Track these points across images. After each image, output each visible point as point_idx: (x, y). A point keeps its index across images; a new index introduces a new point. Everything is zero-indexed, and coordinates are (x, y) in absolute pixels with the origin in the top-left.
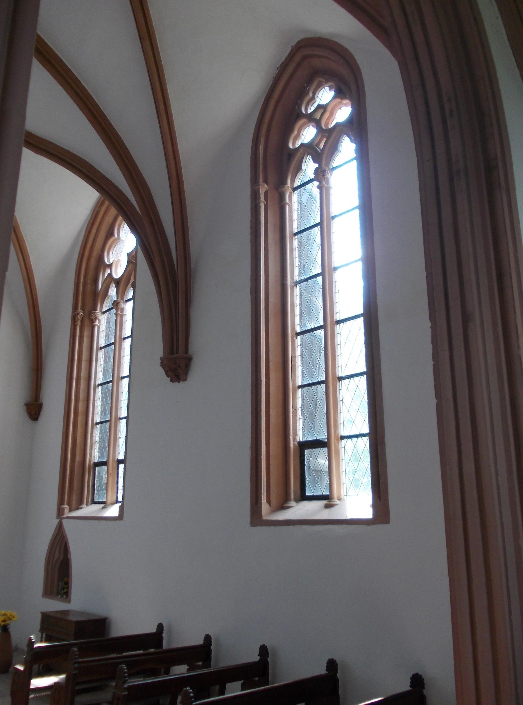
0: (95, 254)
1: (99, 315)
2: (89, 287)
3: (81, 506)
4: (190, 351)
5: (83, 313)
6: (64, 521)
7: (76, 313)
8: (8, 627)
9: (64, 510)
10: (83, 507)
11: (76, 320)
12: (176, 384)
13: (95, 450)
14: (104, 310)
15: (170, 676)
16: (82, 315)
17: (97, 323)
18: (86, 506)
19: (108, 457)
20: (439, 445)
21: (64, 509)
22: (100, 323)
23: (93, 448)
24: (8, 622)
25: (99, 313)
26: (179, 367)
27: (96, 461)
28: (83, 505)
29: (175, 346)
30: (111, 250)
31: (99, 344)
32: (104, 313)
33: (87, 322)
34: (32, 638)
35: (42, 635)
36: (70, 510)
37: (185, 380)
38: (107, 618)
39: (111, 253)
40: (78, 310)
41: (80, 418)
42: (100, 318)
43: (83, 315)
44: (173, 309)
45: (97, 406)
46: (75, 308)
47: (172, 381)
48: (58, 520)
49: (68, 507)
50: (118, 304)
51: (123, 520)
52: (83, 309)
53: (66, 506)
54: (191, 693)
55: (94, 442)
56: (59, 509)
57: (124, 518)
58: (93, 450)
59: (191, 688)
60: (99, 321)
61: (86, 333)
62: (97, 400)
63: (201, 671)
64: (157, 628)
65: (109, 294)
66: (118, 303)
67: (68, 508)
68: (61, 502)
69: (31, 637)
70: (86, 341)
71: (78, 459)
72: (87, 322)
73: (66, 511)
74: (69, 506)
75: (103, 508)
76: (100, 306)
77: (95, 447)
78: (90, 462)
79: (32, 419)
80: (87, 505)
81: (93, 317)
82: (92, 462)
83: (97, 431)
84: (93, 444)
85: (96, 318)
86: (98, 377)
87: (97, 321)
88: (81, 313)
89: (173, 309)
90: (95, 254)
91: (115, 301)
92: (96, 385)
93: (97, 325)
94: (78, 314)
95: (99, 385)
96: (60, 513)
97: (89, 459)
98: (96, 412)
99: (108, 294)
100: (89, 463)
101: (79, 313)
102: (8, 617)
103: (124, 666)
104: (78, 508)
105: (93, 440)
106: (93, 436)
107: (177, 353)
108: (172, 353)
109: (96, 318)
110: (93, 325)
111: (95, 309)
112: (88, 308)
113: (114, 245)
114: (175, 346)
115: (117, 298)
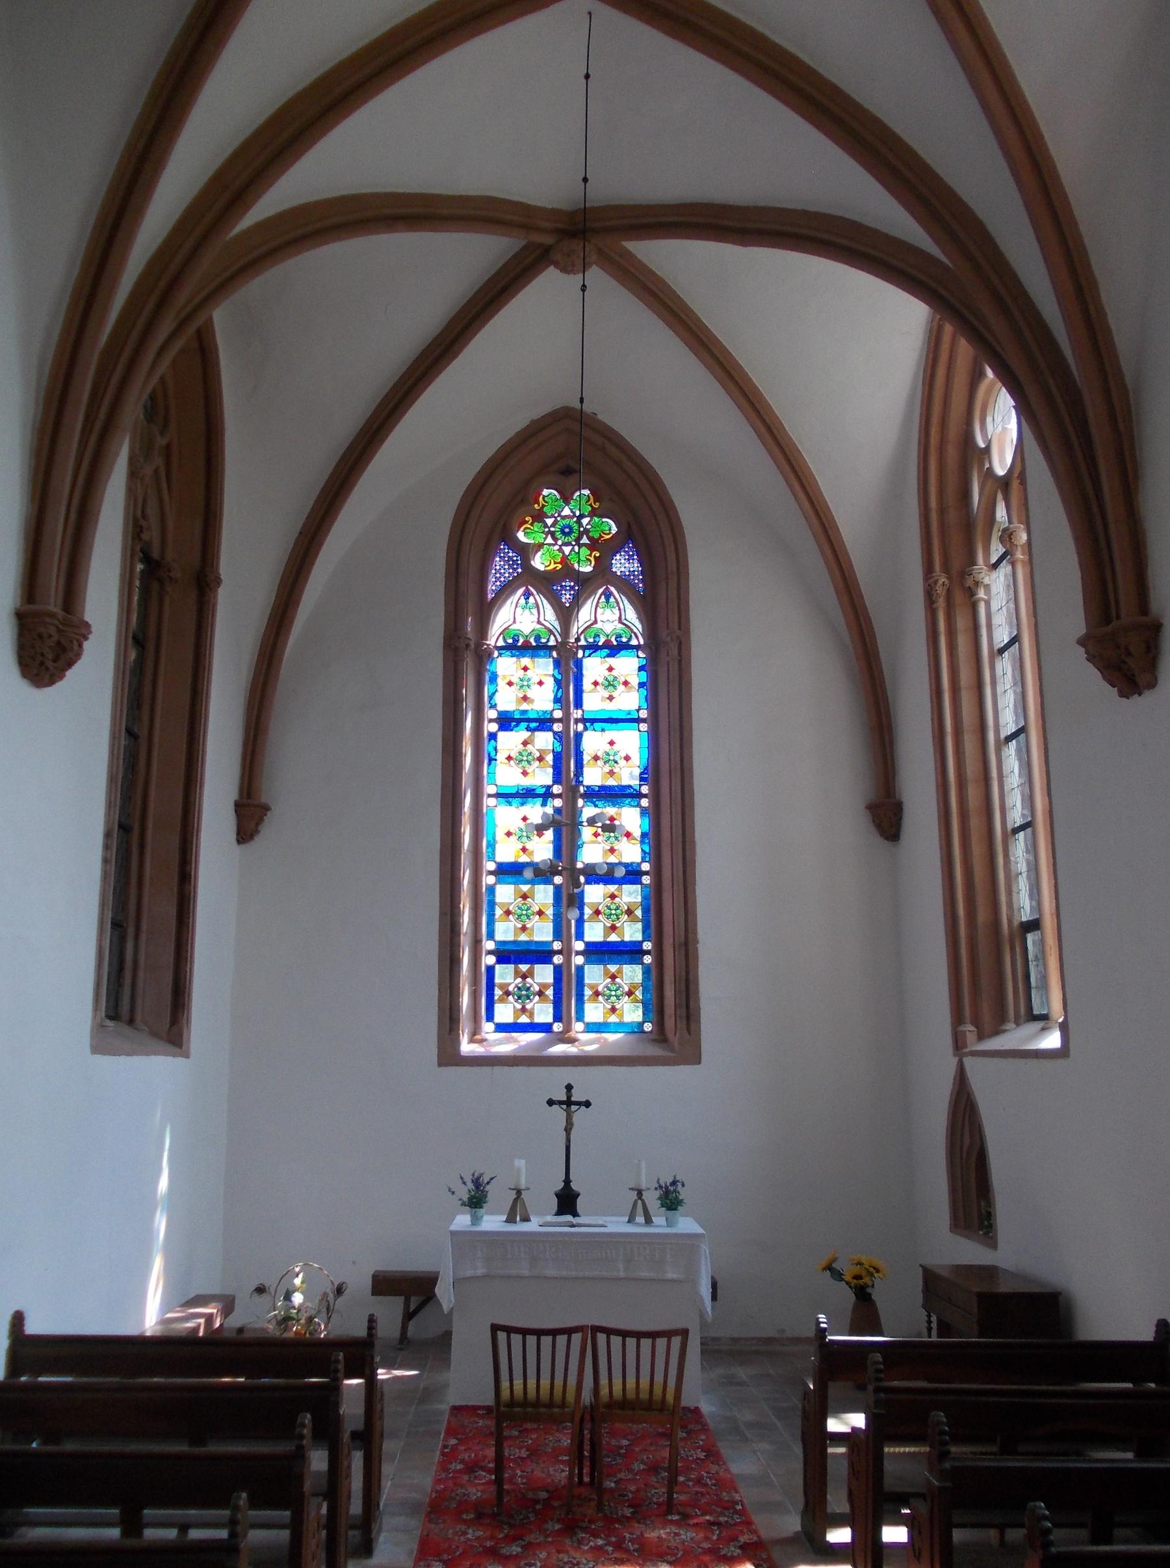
0: (953, 432)
1: (982, 575)
2: (953, 516)
3: (1004, 1027)
4: (1154, 607)
5: (947, 578)
6: (968, 1061)
7: (931, 581)
8: (869, 1290)
9: (966, 1036)
10: (1008, 1028)
11: (934, 599)
12: (1136, 698)
13: (1018, 893)
14: (994, 560)
15: (1084, 1461)
16: (944, 582)
17: (981, 594)
18: (1014, 1026)
19: (1039, 907)
20: (689, 622)
21: (964, 1033)
22: (990, 593)
23: (1014, 889)
24: (867, 1280)
25: (982, 569)
26: (1129, 654)
27: (1024, 919)
28: (1008, 1024)
29: (1113, 603)
30: (988, 413)
31: (994, 643)
32: (995, 566)
33: (959, 597)
34: (821, 1320)
35: (929, 1316)
36: (981, 1037)
37: (1152, 685)
38: (1060, 1293)
39: (989, 419)
40: (934, 574)
41: (975, 823)
42: (986, 581)
43: (947, 582)
44: (1095, 509)
45: (1010, 788)
46: (928, 570)
47: (1123, 694)
48: (956, 1060)
49: (972, 1028)
50: (1012, 537)
51: (1069, 1057)
52: (946, 568)
53: (969, 1028)
54: (1046, 1518)
55: (1013, 874)
56: (956, 1033)
57: (1071, 1052)
58: (1014, 894)
59: (1048, 1508)
60: (987, 588)
61: (962, 623)
62: (1007, 777)
63: (1063, 1461)
64: (1156, 1331)
65: (997, 519)
66: (1011, 534)
67: (975, 1032)
68: (958, 1018)
69: (820, 1316)
70: (963, 642)
71: (982, 916)
72: (959, 597)
73: (971, 1037)
74: (977, 1027)
75: (1043, 1029)
76: (983, 554)
77: (1018, 886)
78: (1010, 921)
79: (887, 839)
80: (1018, 1024)
81: (969, 582)
82: (1016, 923)
83: (1019, 846)
84: (1013, 880)
85: (977, 584)
86: (1002, 722)
87: (982, 590)
88: (943, 579)
89: (1095, 509)
90: (953, 432)
91: (1005, 530)
92: (1000, 741)
93: (983, 599)
94: (936, 582)
95: (1009, 739)
96: (959, 1044)
97: (1007, 915)
98: (1009, 802)
99: (995, 519)
100: (1008, 926)
101: (937, 580)
102: (866, 1268)
103: (941, 1416)
104: (997, 1032)
105: (1010, 870)
106: (1010, 861)
107: (1118, 617)
108: (1107, 620)
109: (977, 584)
110: (972, 600)
111: (972, 562)
112: (956, 563)
113: (992, 400)
114: (1113, 603)
115: (1010, 522)
